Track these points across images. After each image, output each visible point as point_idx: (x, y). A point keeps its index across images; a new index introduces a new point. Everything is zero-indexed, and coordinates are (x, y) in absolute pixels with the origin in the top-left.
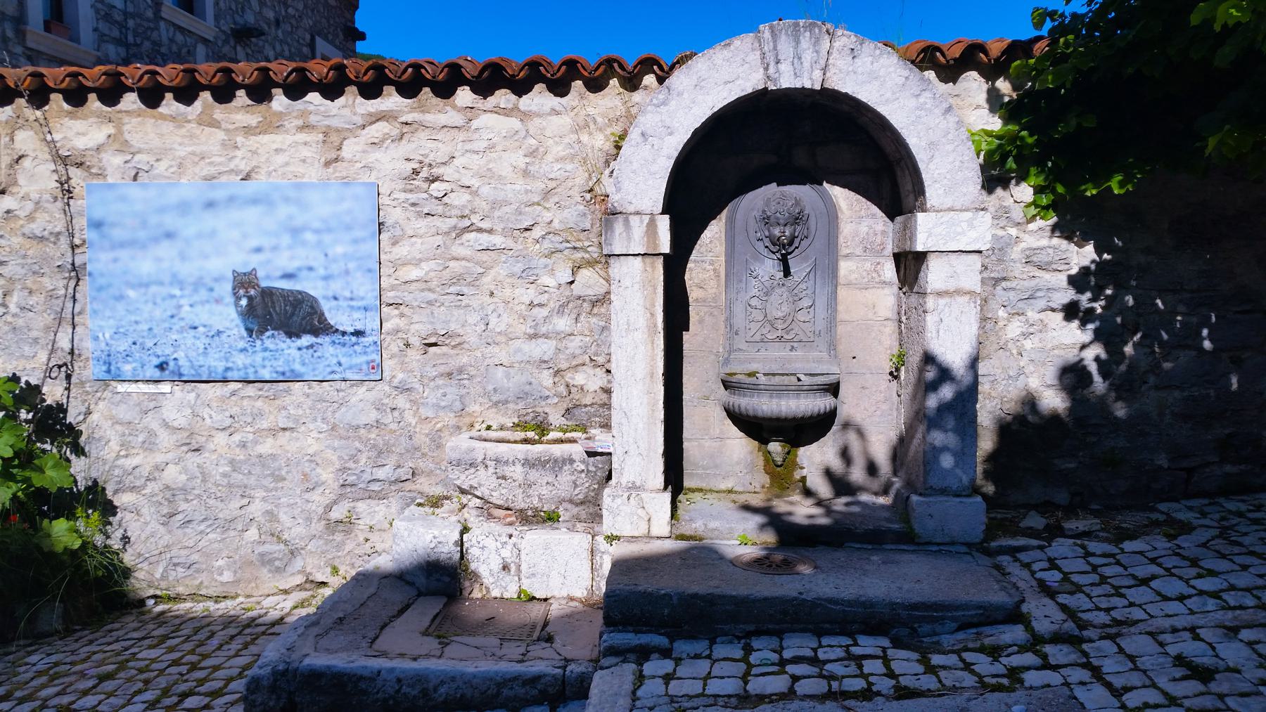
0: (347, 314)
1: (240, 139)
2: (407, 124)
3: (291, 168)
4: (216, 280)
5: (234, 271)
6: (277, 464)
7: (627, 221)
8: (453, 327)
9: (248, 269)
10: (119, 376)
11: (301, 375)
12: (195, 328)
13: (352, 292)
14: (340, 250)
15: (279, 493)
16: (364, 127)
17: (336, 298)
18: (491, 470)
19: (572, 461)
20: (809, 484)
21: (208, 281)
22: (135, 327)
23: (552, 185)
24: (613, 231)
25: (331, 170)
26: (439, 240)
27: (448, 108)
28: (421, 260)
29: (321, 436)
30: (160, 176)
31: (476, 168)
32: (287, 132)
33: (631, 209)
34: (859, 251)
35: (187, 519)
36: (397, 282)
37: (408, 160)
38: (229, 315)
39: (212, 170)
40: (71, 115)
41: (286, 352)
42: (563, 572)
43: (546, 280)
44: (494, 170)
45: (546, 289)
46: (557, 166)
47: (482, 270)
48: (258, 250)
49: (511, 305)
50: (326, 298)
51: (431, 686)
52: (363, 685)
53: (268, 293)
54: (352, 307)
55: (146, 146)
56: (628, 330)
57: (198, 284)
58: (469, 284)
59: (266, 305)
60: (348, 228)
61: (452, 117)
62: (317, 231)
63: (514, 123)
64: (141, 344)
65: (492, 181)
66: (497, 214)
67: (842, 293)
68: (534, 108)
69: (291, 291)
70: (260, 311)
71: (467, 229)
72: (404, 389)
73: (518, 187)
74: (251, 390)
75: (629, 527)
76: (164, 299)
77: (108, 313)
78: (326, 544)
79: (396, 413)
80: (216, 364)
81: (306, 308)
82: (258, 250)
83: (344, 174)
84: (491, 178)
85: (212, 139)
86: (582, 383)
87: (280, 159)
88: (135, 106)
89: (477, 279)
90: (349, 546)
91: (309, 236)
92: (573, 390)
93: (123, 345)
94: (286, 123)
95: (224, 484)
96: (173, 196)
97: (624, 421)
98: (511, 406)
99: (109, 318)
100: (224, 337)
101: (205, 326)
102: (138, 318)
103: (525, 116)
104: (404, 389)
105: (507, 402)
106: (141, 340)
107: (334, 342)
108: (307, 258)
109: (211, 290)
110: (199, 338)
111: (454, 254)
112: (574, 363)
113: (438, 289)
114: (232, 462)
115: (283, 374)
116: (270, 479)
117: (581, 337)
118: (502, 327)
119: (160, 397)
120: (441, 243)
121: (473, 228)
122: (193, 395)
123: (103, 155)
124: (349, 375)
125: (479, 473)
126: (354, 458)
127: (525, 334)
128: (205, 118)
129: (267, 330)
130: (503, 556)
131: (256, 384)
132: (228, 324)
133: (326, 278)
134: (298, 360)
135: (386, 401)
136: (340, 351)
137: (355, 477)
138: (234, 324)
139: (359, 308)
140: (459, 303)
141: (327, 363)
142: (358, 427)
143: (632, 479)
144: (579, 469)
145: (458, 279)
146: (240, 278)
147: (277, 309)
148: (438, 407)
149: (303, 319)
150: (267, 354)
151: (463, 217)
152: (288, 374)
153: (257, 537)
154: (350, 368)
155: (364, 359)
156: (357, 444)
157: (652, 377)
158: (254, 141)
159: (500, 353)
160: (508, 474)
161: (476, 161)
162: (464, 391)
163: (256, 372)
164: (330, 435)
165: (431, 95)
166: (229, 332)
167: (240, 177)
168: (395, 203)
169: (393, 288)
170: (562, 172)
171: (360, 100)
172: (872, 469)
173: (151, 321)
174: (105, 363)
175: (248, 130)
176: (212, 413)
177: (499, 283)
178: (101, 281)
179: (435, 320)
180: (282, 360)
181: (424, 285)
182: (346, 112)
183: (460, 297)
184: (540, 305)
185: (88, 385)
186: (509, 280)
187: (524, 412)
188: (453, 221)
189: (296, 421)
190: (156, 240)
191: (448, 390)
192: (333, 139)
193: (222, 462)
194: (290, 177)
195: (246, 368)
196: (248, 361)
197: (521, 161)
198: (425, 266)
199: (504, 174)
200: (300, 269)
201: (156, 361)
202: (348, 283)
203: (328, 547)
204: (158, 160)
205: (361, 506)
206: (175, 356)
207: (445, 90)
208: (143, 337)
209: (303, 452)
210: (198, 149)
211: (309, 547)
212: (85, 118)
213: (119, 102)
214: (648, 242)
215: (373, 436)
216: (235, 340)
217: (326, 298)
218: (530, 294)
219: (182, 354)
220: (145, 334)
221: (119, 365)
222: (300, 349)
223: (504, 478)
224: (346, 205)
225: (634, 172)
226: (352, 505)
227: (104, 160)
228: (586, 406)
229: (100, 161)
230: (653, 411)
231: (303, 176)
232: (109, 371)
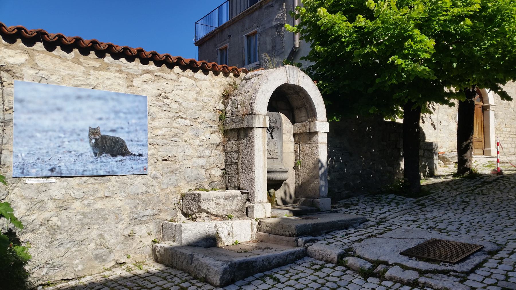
0: (136, 147)
1: (92, 72)
2: (157, 76)
3: (113, 87)
4: (81, 131)
5: (89, 127)
6: (104, 213)
7: (259, 116)
8: (174, 153)
9: (96, 127)
10: (28, 175)
11: (116, 173)
12: (70, 152)
13: (138, 138)
14: (134, 121)
15: (105, 225)
16: (141, 75)
17: (132, 141)
18: (214, 201)
19: (237, 196)
20: (277, 202)
21: (77, 131)
22: (39, 151)
23: (205, 104)
25: (129, 89)
26: (169, 120)
28: (162, 127)
29: (123, 199)
30: (53, 82)
31: (181, 95)
32: (111, 71)
34: (286, 133)
35: (61, 243)
36: (154, 135)
37: (158, 89)
38: (86, 146)
39: (79, 83)
40: (6, 47)
41: (111, 163)
43: (203, 137)
46: (206, 98)
47: (183, 133)
48: (101, 119)
49: (192, 146)
50: (128, 140)
51: (271, 260)
53: (104, 138)
54: (138, 145)
55: (46, 68)
56: (259, 151)
57: (73, 132)
58: (179, 138)
59: (103, 143)
60: (137, 113)
61: (172, 76)
62: (125, 113)
63: (192, 81)
64: (42, 159)
66: (188, 112)
68: (199, 78)
69: (114, 137)
70: (100, 145)
71: (178, 117)
72: (154, 178)
73: (195, 104)
74: (92, 180)
76: (55, 138)
77: (24, 144)
78: (124, 246)
79: (153, 187)
80: (79, 168)
81: (120, 144)
82: (101, 119)
83: (134, 92)
84: (186, 99)
85: (78, 70)
87: (109, 82)
88: (41, 49)
90: (135, 245)
91: (122, 115)
92: (212, 176)
93: (31, 160)
94: (111, 68)
95: (79, 224)
96: (61, 92)
97: (258, 180)
98: (193, 182)
99: (25, 146)
100: (84, 156)
101: (75, 151)
102: (41, 147)
103: (196, 80)
104: (154, 178)
105: (191, 181)
106: (42, 157)
107: (130, 159)
108: (121, 124)
109: (79, 135)
110: (72, 157)
113: (168, 139)
114: (83, 214)
115: (109, 172)
116: (101, 219)
117: (213, 158)
118: (190, 154)
119: (49, 185)
120: (169, 121)
121: (180, 117)
122: (66, 183)
123: (23, 68)
124: (136, 172)
126: (136, 207)
128: (76, 60)
129: (103, 153)
131: (95, 178)
132: (85, 150)
133: (128, 132)
134: (115, 166)
135: (149, 183)
136: (133, 162)
137: (137, 215)
138: (89, 150)
139: (141, 145)
140: (175, 144)
141: (127, 167)
142: (138, 194)
143: (260, 200)
145: (176, 135)
146: (92, 130)
147: (108, 144)
148: (168, 184)
149: (118, 149)
150: (102, 164)
151: (177, 112)
152: (111, 173)
153: (95, 246)
154: (136, 169)
155: (142, 165)
156: (138, 201)
158: (96, 73)
159: (189, 164)
160: (219, 203)
161: (181, 93)
162: (178, 178)
163: (97, 172)
164: (127, 198)
165: (166, 67)
166: (86, 154)
167: (92, 87)
168: (153, 105)
169: (152, 138)
171: (140, 64)
172: (291, 197)
173: (48, 148)
174: (21, 168)
175: (94, 68)
176: (75, 191)
177: (188, 137)
178: (22, 128)
180: (109, 166)
181: (163, 137)
182: (135, 68)
184: (202, 146)
185: (9, 180)
186: (192, 137)
187: (197, 184)
188: (174, 114)
189: (113, 193)
190: (52, 111)
191: (171, 177)
192: (130, 77)
193: (79, 214)
194: (113, 90)
195: (93, 170)
196: (94, 167)
197: (195, 95)
198: (164, 130)
199: (189, 99)
200: (118, 128)
201: (49, 167)
202: (137, 135)
203: (125, 247)
204: (51, 75)
205: (136, 228)
206: (59, 165)
207: (171, 66)
208: (43, 156)
209: (115, 206)
210: (71, 73)
211: (117, 248)
212: (14, 49)
213: (33, 45)
215: (144, 197)
216: (89, 158)
217: (128, 140)
218: (198, 142)
219: (63, 164)
220: (45, 154)
221: (29, 170)
222: (116, 162)
223: (218, 204)
224: (136, 104)
226: (133, 228)
227: (24, 71)
228: (215, 182)
229: (22, 71)
231: (119, 90)
232: (22, 173)
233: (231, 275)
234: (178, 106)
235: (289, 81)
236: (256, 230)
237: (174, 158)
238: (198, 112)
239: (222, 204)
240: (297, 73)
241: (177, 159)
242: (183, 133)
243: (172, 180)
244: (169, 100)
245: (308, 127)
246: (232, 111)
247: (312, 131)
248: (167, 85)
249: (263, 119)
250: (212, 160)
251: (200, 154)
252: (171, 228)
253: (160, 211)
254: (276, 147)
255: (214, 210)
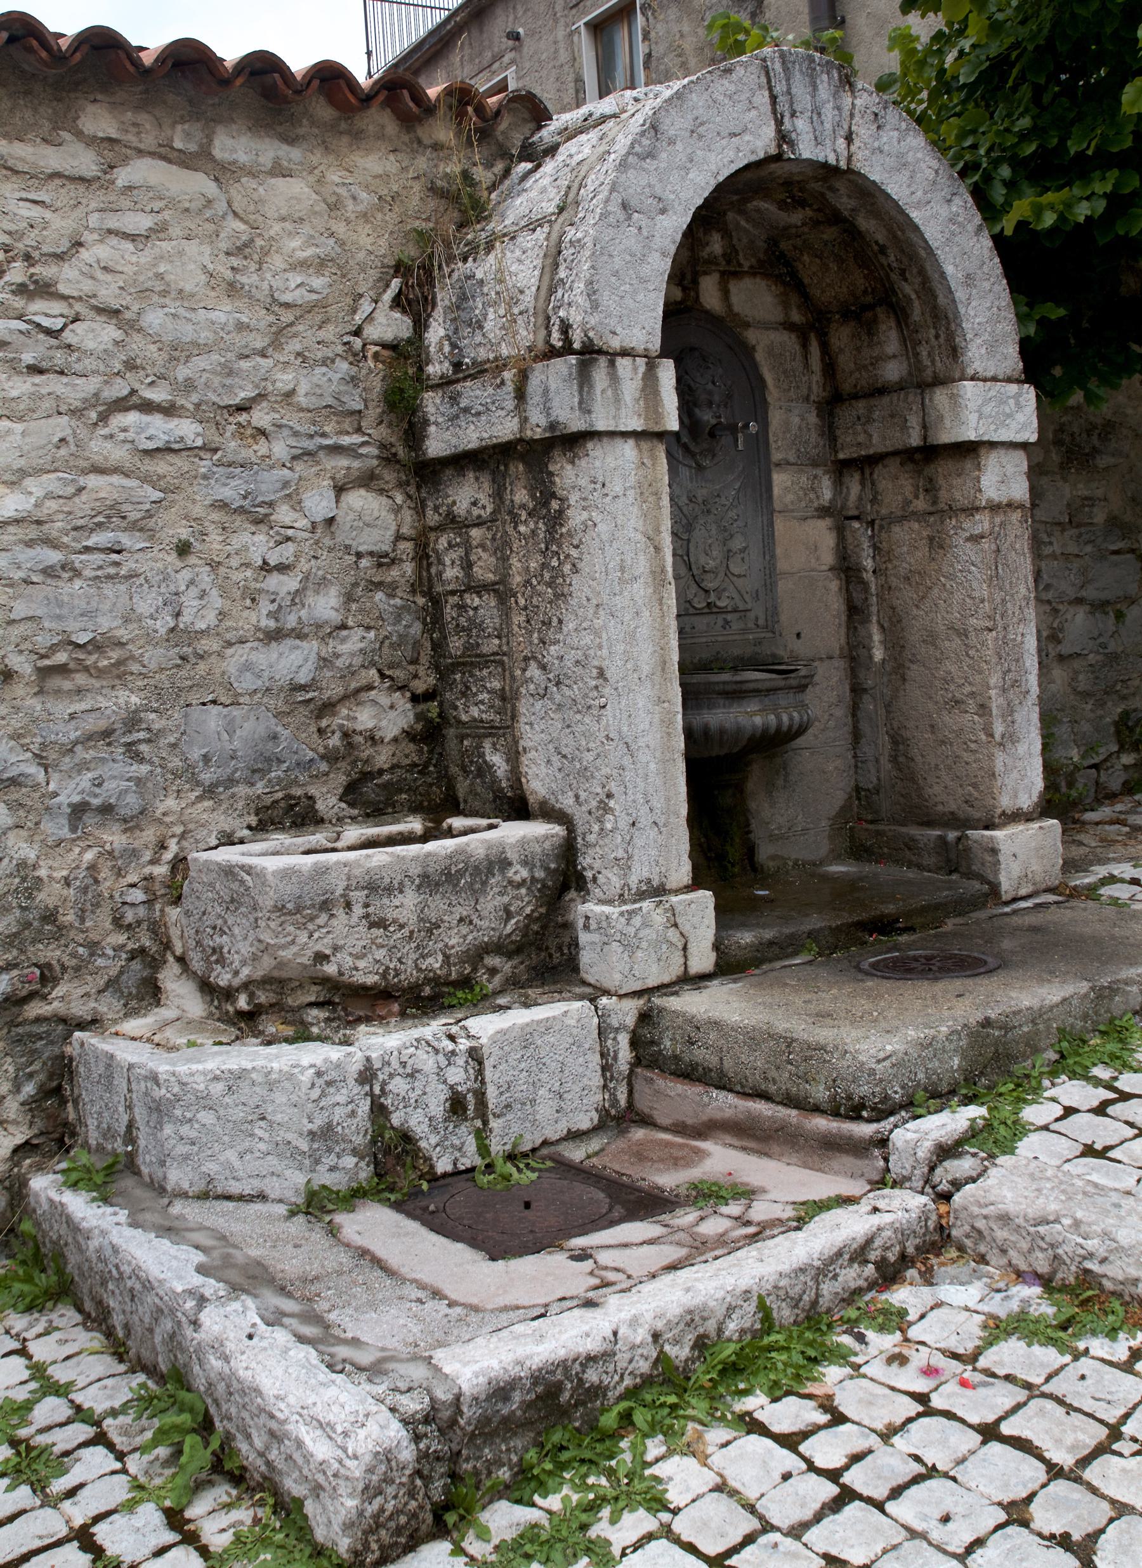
7: (612, 364)
18: (358, 910)
24: (591, 387)
26: (62, 426)
27: (65, 135)
28: (23, 473)
31: (129, 270)
33: (615, 344)
42: (556, 1086)
44: (168, 278)
45: (290, 532)
46: (296, 279)
47: (157, 495)
49: (222, 570)
52: (592, 1376)
63: (198, 184)
65: (167, 301)
67: (779, 524)
68: (243, 158)
71: (121, 405)
73: (219, 316)
75: (654, 968)
84: (164, 293)
86: (370, 725)
89: (149, 515)
97: (627, 761)
103: (223, 173)
105: (231, 782)
111: (98, 459)
112: (354, 685)
125: (334, 922)
127: (258, 629)
130: (451, 1080)
143: (645, 874)
144: (518, 878)
157: (663, 670)
160: (390, 915)
170: (302, 291)
179: (65, 611)
181: (33, 532)
183: (115, 557)
184: (282, 568)
186: (215, 516)
187: (268, 800)
188: (88, 386)
191: (104, 771)
198: (36, 486)
199: (188, 287)
214: (647, 408)
225: (616, 274)
228: (381, 772)
230: (669, 734)
233: (427, 1480)
234: (118, 334)
235: (792, 144)
236: (625, 1054)
237: (115, 655)
238: (244, 364)
239: (414, 918)
240: (836, 95)
241: (132, 657)
242: (157, 495)
243: (110, 785)
244: (57, 307)
245: (914, 421)
246: (454, 346)
247: (946, 437)
248: (35, 212)
249: (638, 382)
250: (352, 644)
251: (273, 615)
252: (110, 1078)
253: (48, 976)
254: (737, 543)
255: (361, 964)
